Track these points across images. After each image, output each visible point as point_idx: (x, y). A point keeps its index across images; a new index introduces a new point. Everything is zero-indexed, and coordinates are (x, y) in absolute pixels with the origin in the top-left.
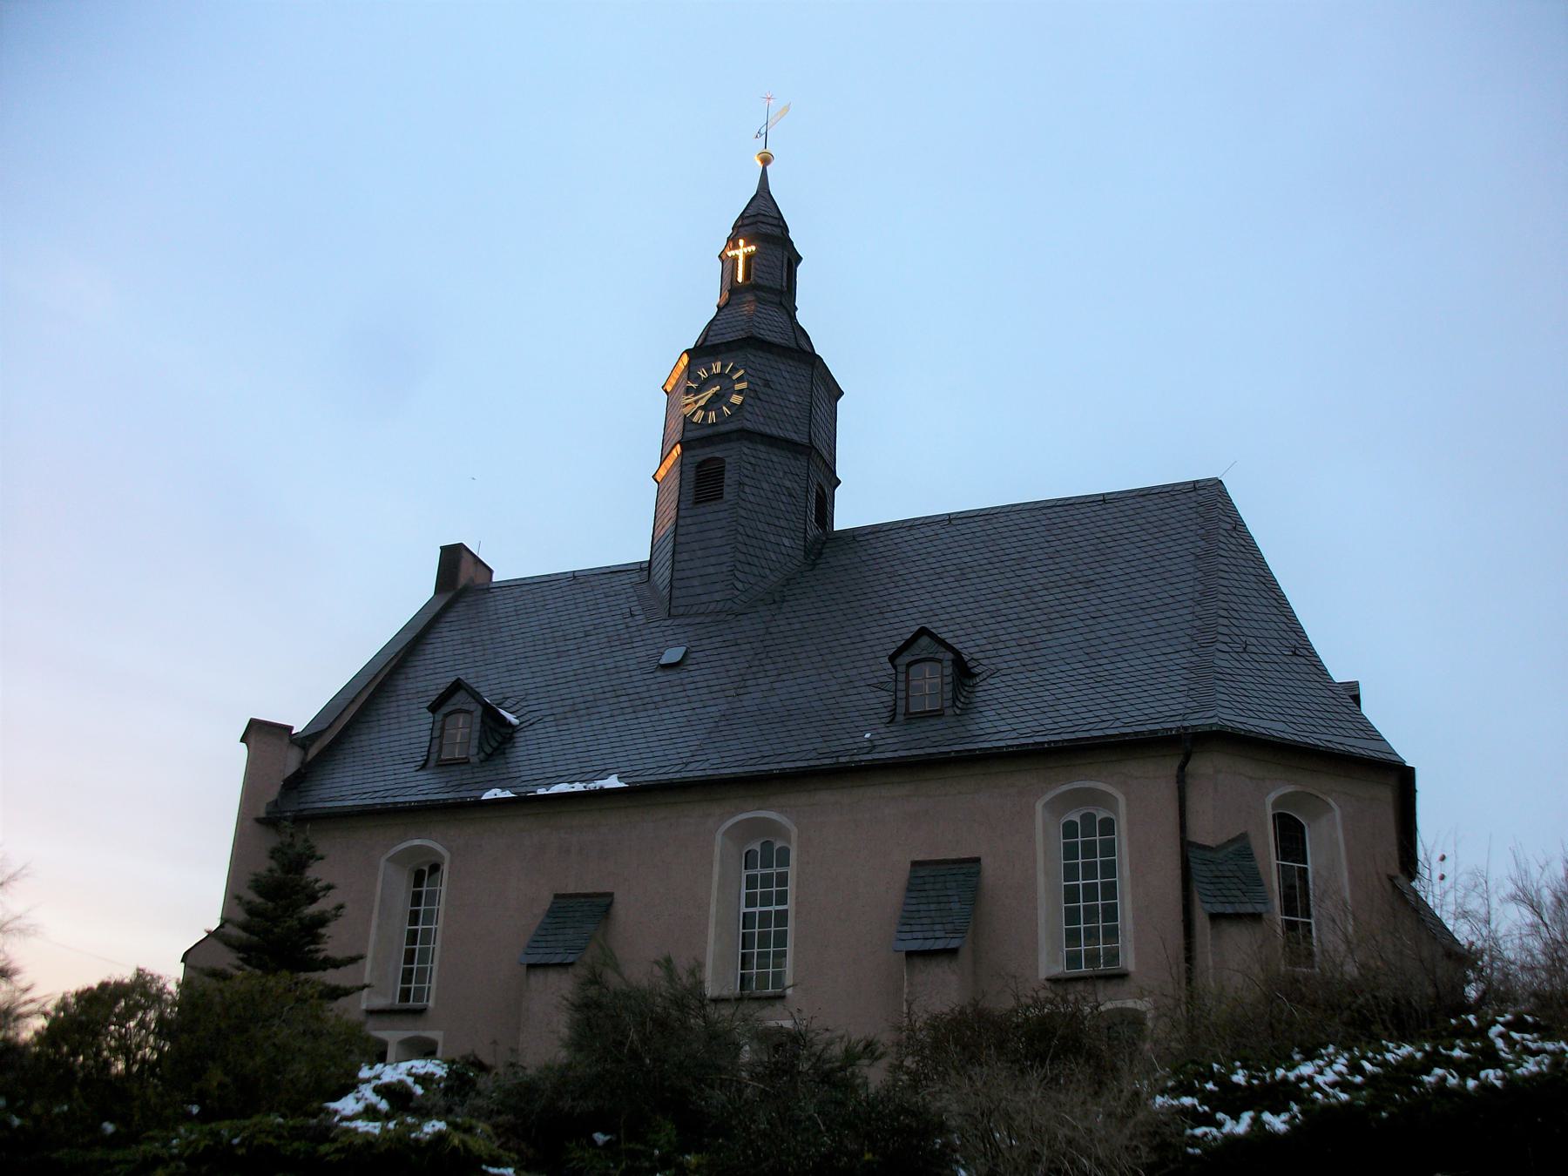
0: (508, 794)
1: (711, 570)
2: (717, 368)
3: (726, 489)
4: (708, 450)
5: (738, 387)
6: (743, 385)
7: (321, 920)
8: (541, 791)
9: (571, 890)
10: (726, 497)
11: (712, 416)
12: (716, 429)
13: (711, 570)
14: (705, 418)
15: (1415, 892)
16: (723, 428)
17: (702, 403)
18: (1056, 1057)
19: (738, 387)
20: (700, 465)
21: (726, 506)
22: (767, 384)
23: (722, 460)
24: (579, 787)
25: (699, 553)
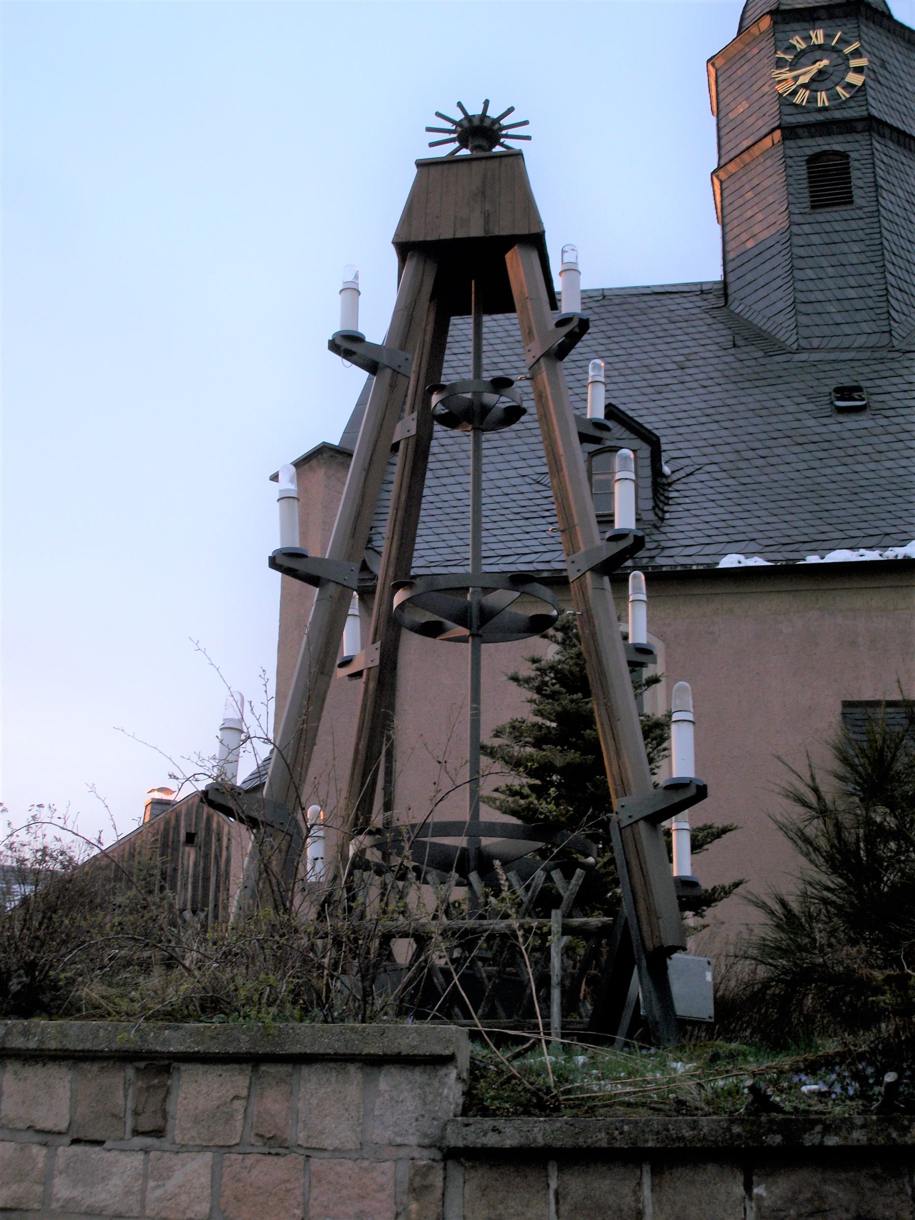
0: (757, 561)
1: (852, 293)
2: (818, 37)
3: (856, 192)
4: (820, 140)
5: (854, 63)
6: (862, 62)
7: (541, 739)
8: (813, 559)
9: (867, 696)
10: (858, 201)
11: (822, 99)
12: (827, 115)
13: (852, 293)
14: (812, 99)
15: (84, 864)
16: (838, 115)
17: (804, 79)
18: (150, 1009)
19: (854, 63)
20: (812, 160)
21: (860, 213)
22: (883, 64)
23: (844, 155)
24: (872, 556)
25: (831, 272)
